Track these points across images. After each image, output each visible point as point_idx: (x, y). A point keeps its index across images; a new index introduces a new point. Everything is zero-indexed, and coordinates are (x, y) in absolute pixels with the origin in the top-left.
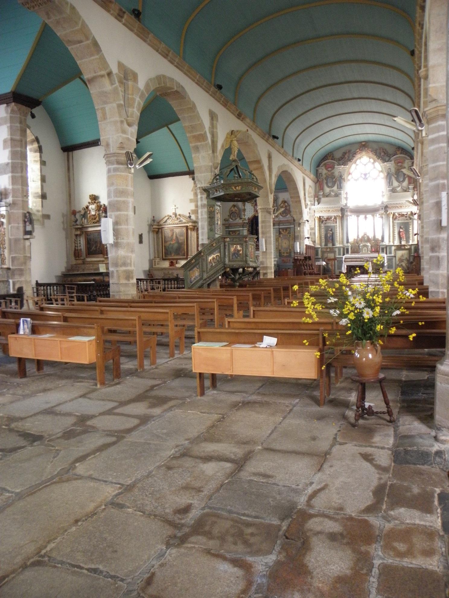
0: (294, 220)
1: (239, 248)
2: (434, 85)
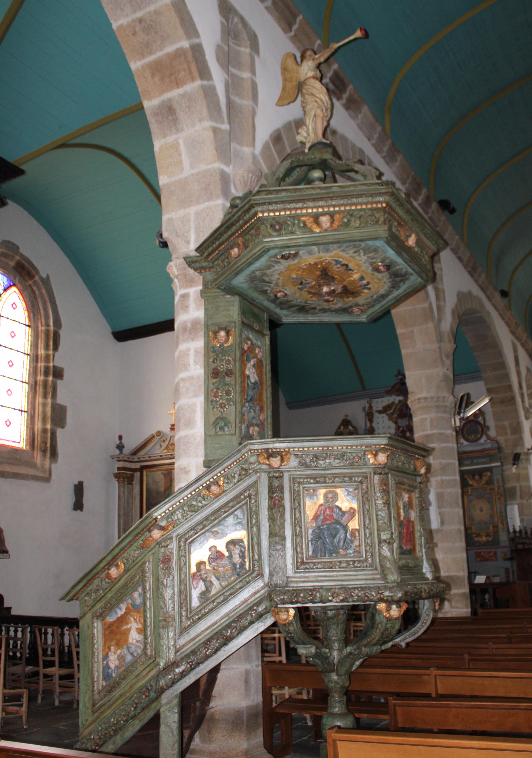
0: (499, 448)
1: (346, 501)
2: (212, 203)
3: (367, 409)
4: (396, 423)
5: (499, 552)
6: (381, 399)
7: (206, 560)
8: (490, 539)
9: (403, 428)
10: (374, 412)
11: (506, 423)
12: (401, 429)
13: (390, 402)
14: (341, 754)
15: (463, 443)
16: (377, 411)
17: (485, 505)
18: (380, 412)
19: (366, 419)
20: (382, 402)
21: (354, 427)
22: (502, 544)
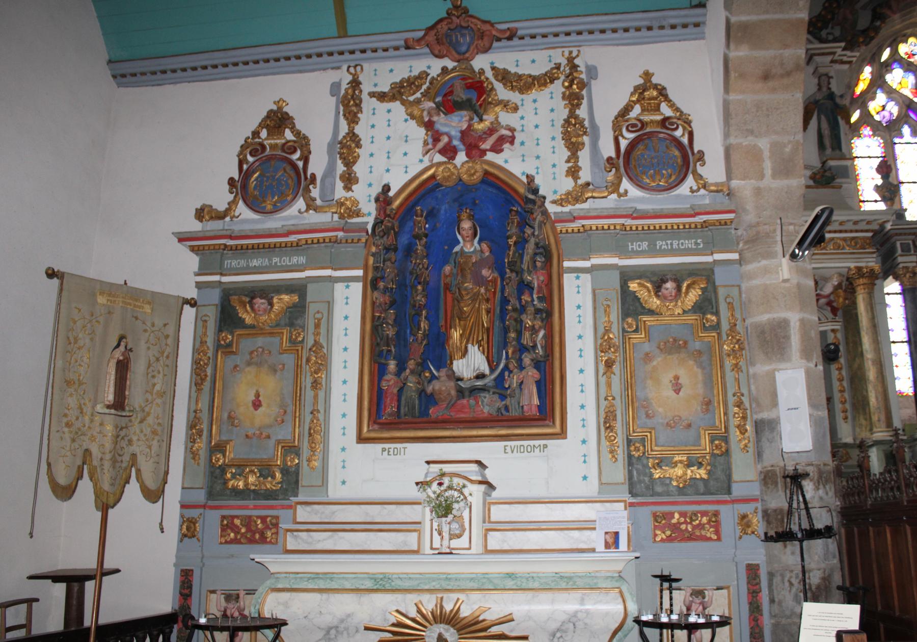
3: (344, 86)
4: (429, 126)
5: (728, 515)
6: (389, 65)
8: (702, 473)
9: (451, 138)
10: (365, 96)
11: (764, 144)
12: (445, 139)
13: (415, 73)
14: (216, 639)
15: (626, 192)
16: (372, 95)
17: (689, 374)
18: (382, 97)
19: (338, 113)
21: (298, 133)
22: (738, 491)
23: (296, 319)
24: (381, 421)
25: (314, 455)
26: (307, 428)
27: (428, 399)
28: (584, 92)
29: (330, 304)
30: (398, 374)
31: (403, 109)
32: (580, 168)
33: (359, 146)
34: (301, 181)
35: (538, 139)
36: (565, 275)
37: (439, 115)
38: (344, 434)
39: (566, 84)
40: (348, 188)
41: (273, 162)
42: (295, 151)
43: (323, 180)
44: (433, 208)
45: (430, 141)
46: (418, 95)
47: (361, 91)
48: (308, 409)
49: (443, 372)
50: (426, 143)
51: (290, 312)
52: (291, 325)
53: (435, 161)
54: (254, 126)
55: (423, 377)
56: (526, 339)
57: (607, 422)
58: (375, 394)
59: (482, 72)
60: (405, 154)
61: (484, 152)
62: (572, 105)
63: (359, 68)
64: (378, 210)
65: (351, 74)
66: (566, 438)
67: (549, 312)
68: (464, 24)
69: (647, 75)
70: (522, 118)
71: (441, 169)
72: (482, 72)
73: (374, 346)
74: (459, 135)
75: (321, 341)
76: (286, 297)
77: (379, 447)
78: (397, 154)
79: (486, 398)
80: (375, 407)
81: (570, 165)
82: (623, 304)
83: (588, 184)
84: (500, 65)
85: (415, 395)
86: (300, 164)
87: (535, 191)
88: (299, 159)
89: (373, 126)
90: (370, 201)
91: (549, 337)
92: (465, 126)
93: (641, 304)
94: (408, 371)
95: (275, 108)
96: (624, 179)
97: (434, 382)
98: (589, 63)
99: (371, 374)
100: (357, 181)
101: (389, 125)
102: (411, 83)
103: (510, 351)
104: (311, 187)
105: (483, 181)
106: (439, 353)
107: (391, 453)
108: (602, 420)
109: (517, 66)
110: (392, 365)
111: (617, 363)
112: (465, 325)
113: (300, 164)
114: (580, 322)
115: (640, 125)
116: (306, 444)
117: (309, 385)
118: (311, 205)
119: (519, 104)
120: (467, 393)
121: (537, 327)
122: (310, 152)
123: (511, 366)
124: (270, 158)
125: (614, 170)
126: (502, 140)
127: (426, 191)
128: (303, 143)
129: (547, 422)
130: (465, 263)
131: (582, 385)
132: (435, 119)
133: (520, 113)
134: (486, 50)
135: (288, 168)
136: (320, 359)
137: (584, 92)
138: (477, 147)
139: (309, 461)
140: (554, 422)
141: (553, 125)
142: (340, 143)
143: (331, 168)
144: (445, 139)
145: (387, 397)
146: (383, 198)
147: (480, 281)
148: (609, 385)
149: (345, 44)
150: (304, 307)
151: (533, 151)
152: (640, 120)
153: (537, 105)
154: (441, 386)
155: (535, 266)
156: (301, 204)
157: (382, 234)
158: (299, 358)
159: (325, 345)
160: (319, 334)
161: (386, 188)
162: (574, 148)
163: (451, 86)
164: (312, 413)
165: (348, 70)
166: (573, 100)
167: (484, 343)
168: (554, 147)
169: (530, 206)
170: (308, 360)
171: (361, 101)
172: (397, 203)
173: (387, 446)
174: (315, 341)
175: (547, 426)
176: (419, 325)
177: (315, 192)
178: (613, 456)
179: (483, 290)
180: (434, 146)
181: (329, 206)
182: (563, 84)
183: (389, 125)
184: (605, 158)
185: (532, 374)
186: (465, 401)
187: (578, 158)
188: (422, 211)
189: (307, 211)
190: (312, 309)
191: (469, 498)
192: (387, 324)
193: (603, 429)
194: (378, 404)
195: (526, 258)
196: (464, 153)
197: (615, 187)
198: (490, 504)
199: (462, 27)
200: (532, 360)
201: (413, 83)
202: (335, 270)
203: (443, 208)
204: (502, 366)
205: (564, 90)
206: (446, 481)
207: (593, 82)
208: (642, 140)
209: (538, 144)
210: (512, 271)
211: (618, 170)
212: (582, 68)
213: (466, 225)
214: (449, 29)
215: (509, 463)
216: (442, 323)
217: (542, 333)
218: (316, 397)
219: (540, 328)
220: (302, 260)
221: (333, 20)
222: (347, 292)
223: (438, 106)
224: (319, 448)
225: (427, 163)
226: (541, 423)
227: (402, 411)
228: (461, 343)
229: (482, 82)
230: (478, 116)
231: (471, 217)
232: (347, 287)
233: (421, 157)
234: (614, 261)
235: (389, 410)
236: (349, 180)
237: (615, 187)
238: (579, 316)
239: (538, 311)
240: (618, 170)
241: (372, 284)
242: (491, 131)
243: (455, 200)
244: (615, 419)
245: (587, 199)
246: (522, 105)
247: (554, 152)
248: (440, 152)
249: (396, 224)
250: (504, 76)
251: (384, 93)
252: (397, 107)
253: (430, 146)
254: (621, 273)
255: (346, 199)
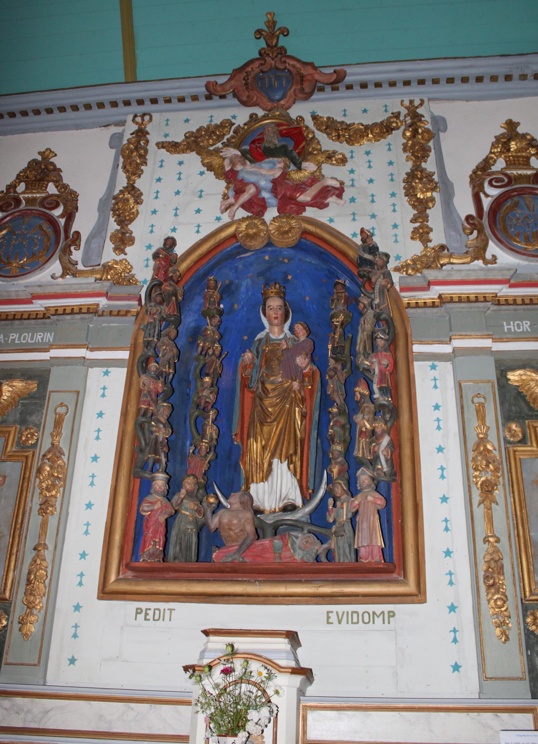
4: (230, 176)
7: (428, 224)
9: (259, 190)
10: (152, 147)
12: (251, 190)
13: (217, 121)
15: (494, 258)
16: (161, 145)
18: (173, 147)
19: (116, 166)
20: (187, 121)
23: (31, 414)
24: (137, 564)
25: (32, 614)
26: (25, 571)
27: (208, 539)
28: (431, 144)
29: (79, 395)
30: (169, 495)
31: (199, 158)
32: (431, 230)
33: (138, 201)
34: (59, 239)
35: (373, 196)
36: (416, 364)
37: (244, 164)
38: (80, 584)
39: (408, 134)
40: (120, 248)
41: (26, 219)
42: (57, 206)
43: (88, 241)
44: (231, 283)
45: (231, 193)
46: (219, 145)
47: (147, 142)
48: (30, 543)
49: (235, 498)
50: (225, 197)
51: (24, 405)
52: (23, 421)
53: (236, 218)
54: (11, 178)
55: (205, 504)
56: (360, 450)
57: (489, 577)
58: (132, 525)
59: (301, 119)
60: (198, 211)
61: (302, 206)
62: (417, 158)
63: (147, 118)
64: (157, 270)
65: (137, 123)
66: (424, 601)
67: (397, 408)
68: (281, 66)
69: (511, 125)
70: (352, 171)
71: (244, 225)
72: (301, 119)
73: (137, 450)
74: (270, 185)
75: (61, 445)
76: (19, 384)
77: (132, 606)
78: (187, 207)
79: (299, 538)
80: (131, 544)
81: (417, 225)
82: (502, 403)
83: (443, 247)
84: (324, 114)
85: (191, 529)
86: (62, 222)
87: (373, 250)
88: (62, 216)
89: (159, 180)
90: (147, 266)
91: (395, 446)
92: (277, 174)
93: (527, 403)
94: (183, 491)
95: (39, 158)
96: (490, 242)
97: (221, 512)
98: (436, 114)
99: (129, 494)
100: (132, 241)
101: (179, 179)
102: (213, 132)
103: (335, 470)
104: (72, 248)
105: (298, 247)
106: (228, 473)
107: (150, 616)
108: (481, 574)
109: (345, 115)
110: (160, 480)
111: (500, 487)
112: (270, 434)
113: (62, 222)
114: (439, 428)
115: (506, 180)
116: (21, 595)
117: (36, 507)
118: (69, 269)
119: (348, 155)
120: (269, 531)
121: (378, 431)
122: (77, 209)
123: (338, 491)
124: (24, 214)
125: (475, 232)
126: (326, 192)
127: (222, 253)
128: (70, 201)
129: (395, 575)
130: (272, 352)
131: (446, 520)
132: (239, 168)
133: (349, 166)
134: (307, 96)
135: (46, 227)
136: (57, 469)
137: (431, 144)
138: (293, 199)
139: (22, 622)
140: (405, 576)
141: (392, 180)
142: (115, 198)
143: (100, 228)
144: (251, 190)
145: (148, 528)
146: (165, 254)
147: (293, 373)
148: (490, 520)
149: (133, 91)
150: (43, 397)
151: (367, 203)
152: (506, 175)
153: (370, 157)
154: (231, 517)
155: (373, 348)
156: (55, 267)
157: (159, 299)
158: (26, 468)
159: (66, 451)
160: (59, 434)
161: (170, 243)
162: (421, 207)
163: (261, 134)
164: (35, 549)
165: (133, 120)
166: (418, 150)
167: (297, 459)
168: (394, 205)
169: (368, 269)
170: (39, 471)
171: (146, 151)
172: (183, 267)
173: (144, 605)
174: (53, 444)
175: (396, 582)
176: (204, 431)
177: (77, 255)
178: (503, 633)
179: (296, 385)
180: (236, 198)
181: (92, 272)
182: (404, 134)
183: (179, 179)
184: (463, 218)
185: (370, 501)
186: (266, 542)
187: (427, 216)
188: (216, 282)
189: (63, 276)
190: (54, 400)
191: (274, 699)
192: (158, 421)
193: (483, 588)
194: (136, 541)
195: (362, 337)
196: (275, 209)
197: (479, 253)
198: (306, 708)
199: (277, 69)
200: (373, 479)
201: (214, 132)
202: (92, 350)
203: (244, 283)
204: (321, 493)
205: (405, 141)
206: (238, 665)
207: (442, 135)
208: (510, 197)
209: (373, 201)
210: (336, 360)
211: (481, 231)
212: (427, 117)
213: (275, 303)
214: (262, 71)
215: (340, 639)
216: (236, 429)
217: (386, 441)
218: (44, 525)
219: (383, 432)
220: (49, 337)
221: (120, 63)
222: (104, 381)
223: (244, 154)
224: (40, 603)
225: (226, 218)
226: (385, 576)
227: (171, 552)
228: (262, 460)
229: (300, 128)
230: (295, 164)
231: (282, 295)
232: (106, 373)
233: (219, 214)
234: (487, 343)
235: (150, 548)
236: (123, 240)
237: (479, 253)
238: (438, 420)
239: (380, 409)
240: (481, 231)
241: (139, 365)
242: (314, 179)
243: (261, 274)
244: (501, 570)
245: (442, 265)
246: (352, 157)
247: (394, 211)
248: (243, 206)
249: (180, 291)
250: (331, 127)
251: (177, 143)
252: (193, 160)
253: (232, 200)
254: (496, 361)
255: (116, 262)
